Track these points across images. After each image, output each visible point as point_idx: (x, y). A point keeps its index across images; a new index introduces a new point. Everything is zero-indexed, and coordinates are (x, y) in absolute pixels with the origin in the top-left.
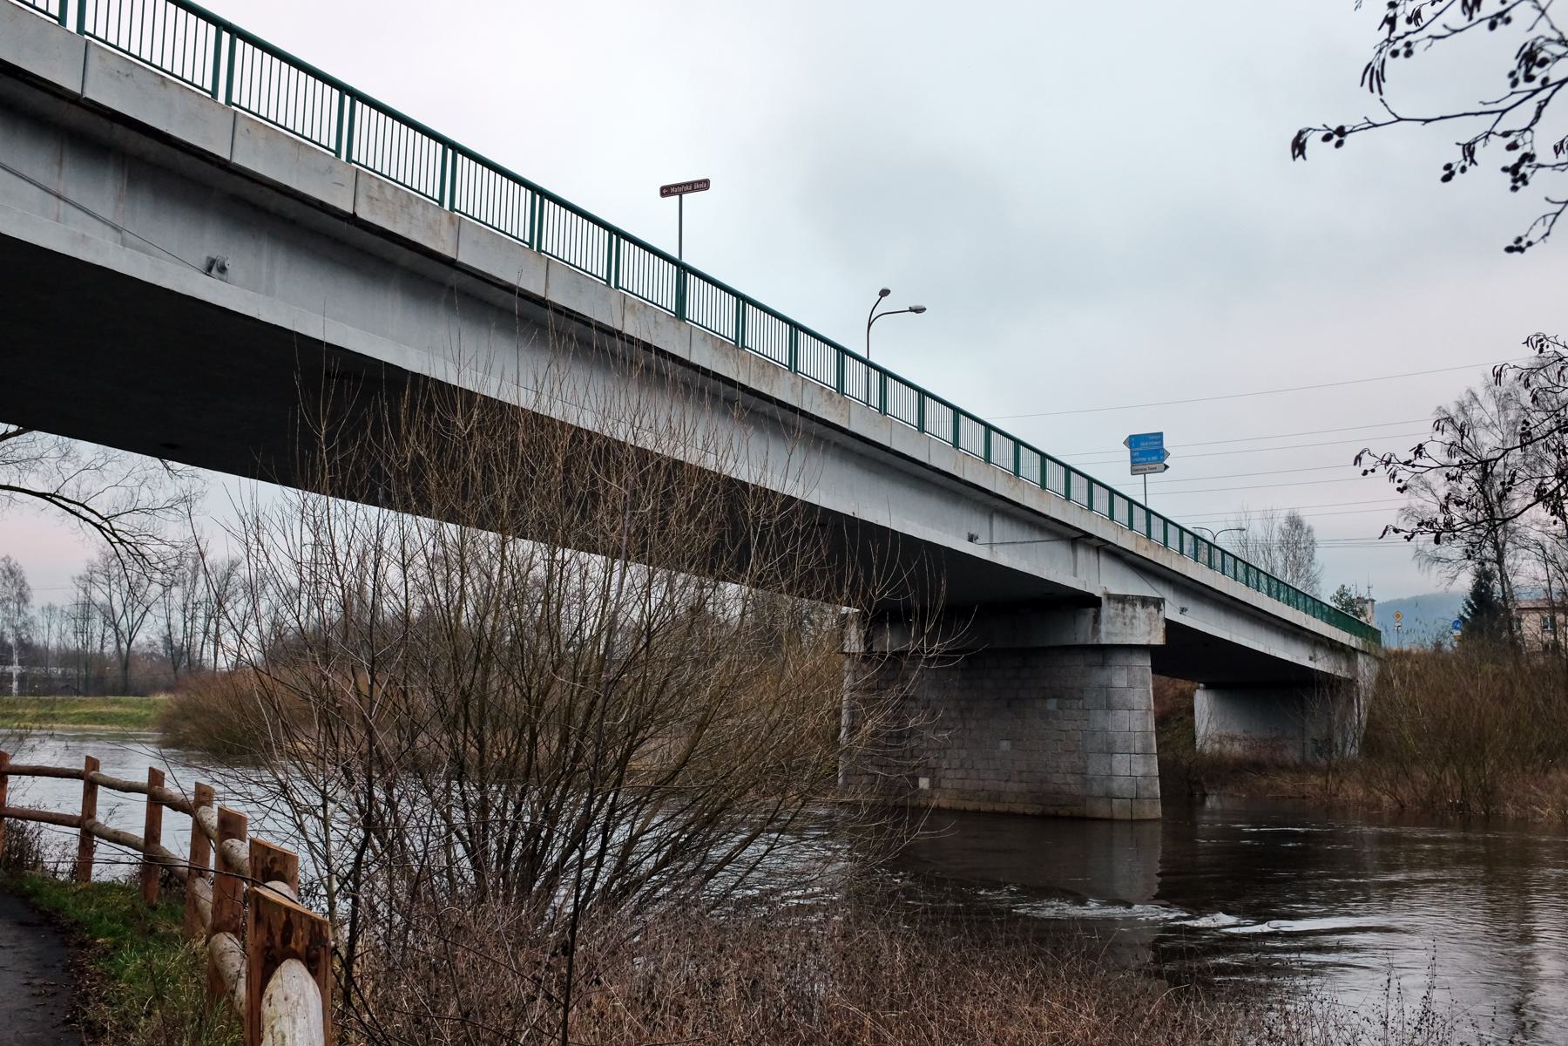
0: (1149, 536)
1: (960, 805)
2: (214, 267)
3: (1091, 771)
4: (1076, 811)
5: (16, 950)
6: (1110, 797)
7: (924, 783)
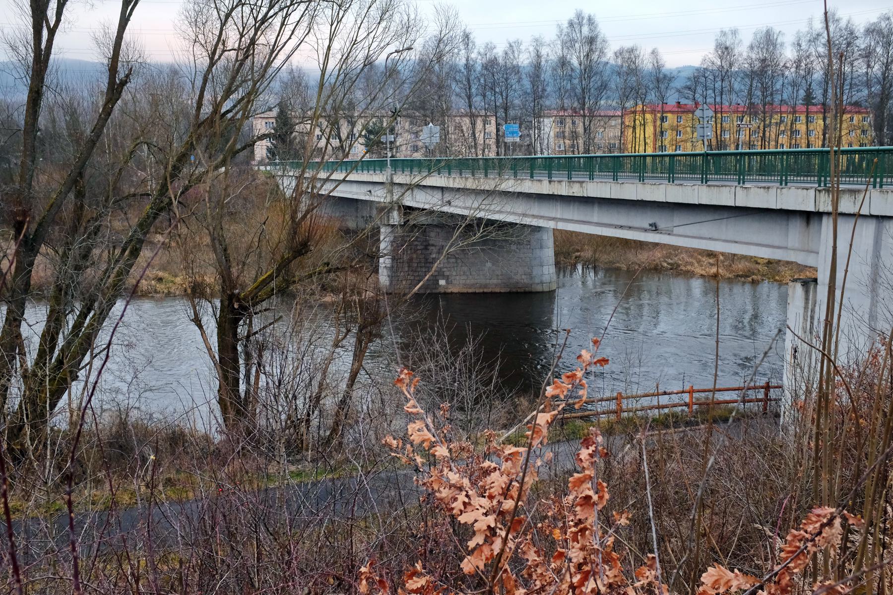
0: (809, 217)
1: (465, 291)
2: (654, 228)
3: (534, 273)
4: (527, 289)
5: (553, 460)
6: (542, 283)
7: (442, 282)
